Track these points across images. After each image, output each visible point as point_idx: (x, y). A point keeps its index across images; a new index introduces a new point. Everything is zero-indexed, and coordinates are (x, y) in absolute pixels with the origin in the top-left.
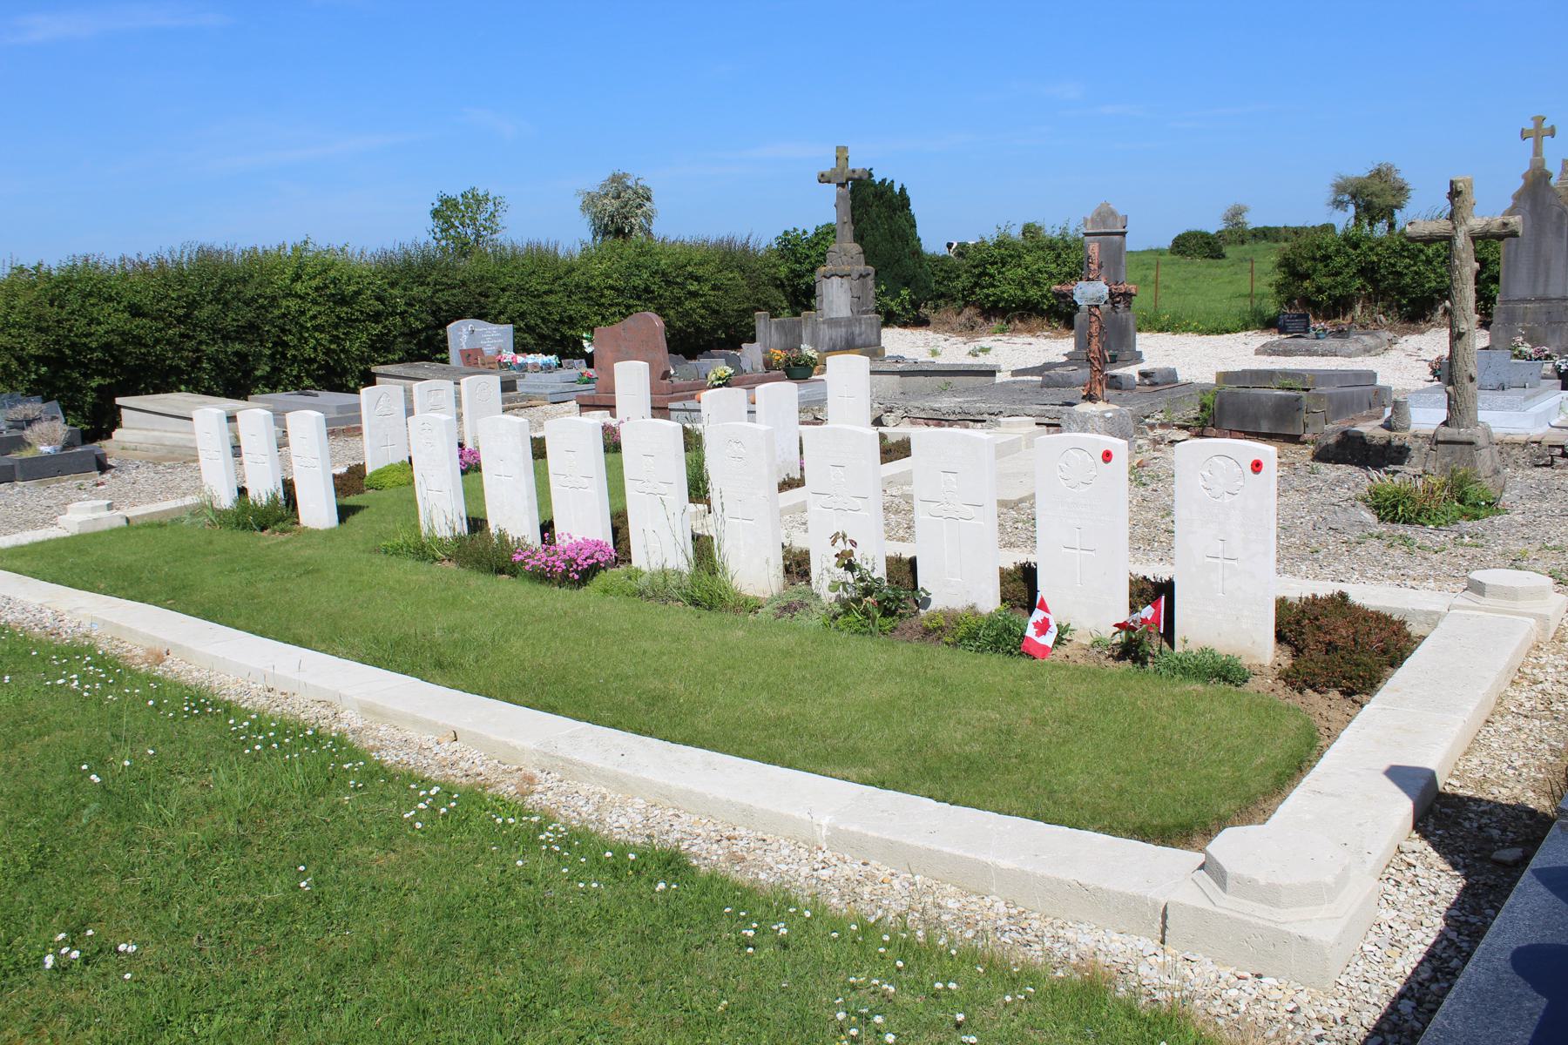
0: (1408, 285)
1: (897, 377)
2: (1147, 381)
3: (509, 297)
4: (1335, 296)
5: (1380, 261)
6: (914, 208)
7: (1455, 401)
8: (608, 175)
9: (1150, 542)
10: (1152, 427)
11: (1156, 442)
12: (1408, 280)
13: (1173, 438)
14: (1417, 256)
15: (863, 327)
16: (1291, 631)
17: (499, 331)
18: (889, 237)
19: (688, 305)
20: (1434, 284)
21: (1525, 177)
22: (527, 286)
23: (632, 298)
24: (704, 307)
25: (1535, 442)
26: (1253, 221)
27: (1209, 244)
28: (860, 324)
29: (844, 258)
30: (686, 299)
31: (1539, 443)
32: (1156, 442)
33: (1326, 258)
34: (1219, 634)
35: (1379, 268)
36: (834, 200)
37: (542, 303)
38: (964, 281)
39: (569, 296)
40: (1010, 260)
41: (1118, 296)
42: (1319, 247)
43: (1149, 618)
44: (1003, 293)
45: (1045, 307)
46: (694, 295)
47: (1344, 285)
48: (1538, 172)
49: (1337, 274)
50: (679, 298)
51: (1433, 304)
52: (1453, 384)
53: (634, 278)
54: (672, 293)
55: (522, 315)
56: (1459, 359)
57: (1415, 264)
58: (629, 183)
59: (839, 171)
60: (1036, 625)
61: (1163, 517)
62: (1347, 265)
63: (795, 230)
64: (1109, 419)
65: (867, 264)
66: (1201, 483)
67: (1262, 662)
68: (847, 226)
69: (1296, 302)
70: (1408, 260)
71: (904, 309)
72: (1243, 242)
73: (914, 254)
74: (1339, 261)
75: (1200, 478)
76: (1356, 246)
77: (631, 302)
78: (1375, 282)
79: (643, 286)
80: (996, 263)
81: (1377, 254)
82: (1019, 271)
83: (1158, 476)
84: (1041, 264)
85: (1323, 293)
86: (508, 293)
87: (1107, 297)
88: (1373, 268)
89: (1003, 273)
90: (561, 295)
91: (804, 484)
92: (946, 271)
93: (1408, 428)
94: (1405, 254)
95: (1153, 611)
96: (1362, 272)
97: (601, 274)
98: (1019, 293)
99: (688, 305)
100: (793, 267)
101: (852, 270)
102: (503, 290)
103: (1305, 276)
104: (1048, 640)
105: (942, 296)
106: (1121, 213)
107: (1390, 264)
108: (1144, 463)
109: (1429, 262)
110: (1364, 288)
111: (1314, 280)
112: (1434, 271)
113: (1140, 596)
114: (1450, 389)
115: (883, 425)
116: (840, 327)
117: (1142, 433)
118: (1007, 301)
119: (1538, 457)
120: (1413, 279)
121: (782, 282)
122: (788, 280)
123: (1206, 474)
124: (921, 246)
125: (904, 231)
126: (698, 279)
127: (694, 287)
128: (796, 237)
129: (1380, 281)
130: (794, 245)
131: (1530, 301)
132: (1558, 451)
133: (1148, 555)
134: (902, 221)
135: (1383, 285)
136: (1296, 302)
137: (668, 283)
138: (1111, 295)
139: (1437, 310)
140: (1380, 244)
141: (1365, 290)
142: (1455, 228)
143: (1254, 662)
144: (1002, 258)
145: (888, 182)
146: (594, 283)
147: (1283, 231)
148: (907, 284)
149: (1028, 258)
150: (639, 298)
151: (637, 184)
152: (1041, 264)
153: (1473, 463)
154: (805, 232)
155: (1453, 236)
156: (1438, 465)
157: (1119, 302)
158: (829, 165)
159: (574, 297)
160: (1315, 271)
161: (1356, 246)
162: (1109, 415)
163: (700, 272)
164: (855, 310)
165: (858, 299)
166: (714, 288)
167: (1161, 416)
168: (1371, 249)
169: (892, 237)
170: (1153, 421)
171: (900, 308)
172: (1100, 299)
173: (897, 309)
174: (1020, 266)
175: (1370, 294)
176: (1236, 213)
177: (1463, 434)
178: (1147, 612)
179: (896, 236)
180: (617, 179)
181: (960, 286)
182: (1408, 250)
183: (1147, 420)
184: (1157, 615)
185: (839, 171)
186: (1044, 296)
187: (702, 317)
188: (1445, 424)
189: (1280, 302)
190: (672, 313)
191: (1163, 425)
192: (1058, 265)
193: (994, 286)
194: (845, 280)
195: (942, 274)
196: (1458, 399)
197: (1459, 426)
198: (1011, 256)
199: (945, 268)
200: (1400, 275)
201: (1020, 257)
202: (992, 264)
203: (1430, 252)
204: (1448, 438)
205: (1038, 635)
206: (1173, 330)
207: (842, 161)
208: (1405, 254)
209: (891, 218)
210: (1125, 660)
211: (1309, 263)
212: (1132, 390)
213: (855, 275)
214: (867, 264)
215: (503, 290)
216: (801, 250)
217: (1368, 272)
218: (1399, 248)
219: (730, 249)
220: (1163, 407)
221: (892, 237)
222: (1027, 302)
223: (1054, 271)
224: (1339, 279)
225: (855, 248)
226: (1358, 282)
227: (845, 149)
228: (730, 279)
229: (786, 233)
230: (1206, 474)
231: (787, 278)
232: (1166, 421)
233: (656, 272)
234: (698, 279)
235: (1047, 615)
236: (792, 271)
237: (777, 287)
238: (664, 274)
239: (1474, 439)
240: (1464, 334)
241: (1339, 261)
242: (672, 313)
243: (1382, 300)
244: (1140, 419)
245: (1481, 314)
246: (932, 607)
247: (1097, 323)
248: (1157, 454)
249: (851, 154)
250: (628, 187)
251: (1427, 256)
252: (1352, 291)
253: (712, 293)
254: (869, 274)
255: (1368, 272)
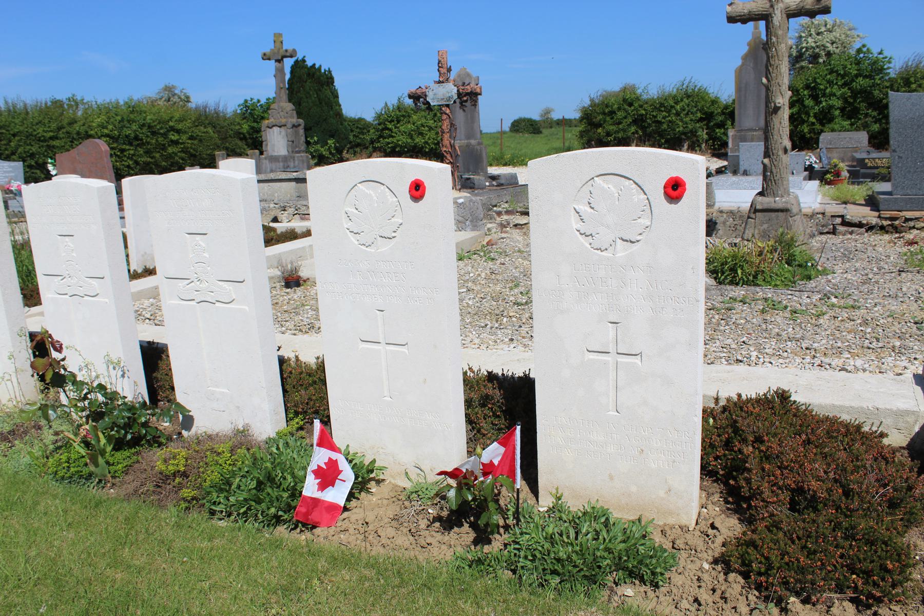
0: (665, 130)
1: (293, 184)
2: (494, 183)
3: (19, 141)
4: (618, 137)
5: (647, 114)
6: (337, 83)
7: (771, 172)
8: (162, 86)
9: (498, 317)
10: (499, 214)
11: (503, 226)
12: (665, 126)
13: (517, 222)
14: (670, 111)
15: (297, 162)
16: (717, 458)
17: (10, 167)
18: (318, 103)
19: (170, 150)
20: (681, 129)
21: (749, 44)
22: (35, 133)
23: (125, 144)
24: (182, 151)
25: (819, 214)
26: (556, 116)
27: (532, 125)
28: (294, 160)
29: (282, 114)
30: (169, 146)
31: (823, 214)
32: (503, 226)
33: (612, 113)
34: (611, 478)
35: (646, 119)
36: (273, 72)
37: (48, 146)
38: (372, 134)
39: (72, 142)
40: (402, 118)
41: (465, 96)
42: (607, 106)
43: (496, 462)
44: (398, 141)
45: (427, 150)
46: (176, 143)
47: (624, 130)
48: (757, 40)
49: (620, 123)
50: (164, 145)
51: (681, 143)
52: (769, 157)
53: (125, 129)
54: (157, 140)
55: (32, 156)
56: (775, 132)
57: (669, 116)
58: (176, 92)
59: (276, 51)
60: (318, 473)
61: (511, 289)
62: (625, 117)
63: (252, 99)
64: (460, 204)
65: (298, 118)
66: (576, 224)
67: (684, 522)
68: (283, 91)
69: (593, 143)
70: (664, 113)
71: (331, 153)
72: (551, 127)
73: (336, 115)
74: (620, 114)
75: (574, 218)
76: (630, 105)
77: (124, 147)
78: (643, 128)
79: (133, 135)
80: (393, 121)
81: (645, 110)
82: (409, 126)
83: (505, 252)
84: (424, 121)
85: (611, 136)
86: (17, 138)
87: (455, 97)
88: (642, 119)
89: (398, 128)
90: (63, 140)
91: (155, 274)
92: (360, 128)
93: (714, 205)
94: (663, 109)
95: (502, 450)
96: (635, 122)
97: (99, 126)
98: (409, 141)
99: (170, 150)
100: (252, 124)
101: (287, 122)
102: (14, 135)
103: (599, 125)
104: (337, 495)
105: (358, 145)
106: (474, 75)
107: (653, 115)
108: (492, 242)
109: (678, 114)
110: (637, 132)
111: (604, 127)
112: (681, 120)
113: (483, 405)
114: (766, 161)
115: (278, 222)
116: (279, 162)
117: (491, 219)
118: (401, 147)
119: (823, 226)
120: (668, 125)
121: (244, 135)
122: (249, 134)
123: (584, 208)
124: (341, 109)
125: (329, 99)
126: (178, 132)
127: (174, 137)
128: (253, 104)
129: (647, 127)
130: (252, 110)
131: (755, 130)
132: (839, 220)
133: (495, 334)
134: (328, 92)
135: (649, 130)
136: (593, 143)
137: (154, 133)
138: (459, 95)
139: (683, 146)
140: (647, 103)
141: (638, 134)
142: (772, 6)
143: (671, 521)
144: (397, 118)
145: (317, 66)
146: (92, 132)
147: (574, 121)
148: (332, 136)
149: (414, 117)
150: (131, 144)
151: (181, 92)
152: (424, 121)
153: (789, 227)
154: (259, 101)
155: (770, 14)
156: (757, 231)
157: (466, 101)
158: (268, 47)
159: (75, 142)
160: (605, 121)
161: (630, 105)
162: (461, 201)
163: (180, 127)
164: (290, 150)
165: (292, 143)
166: (191, 138)
167: (506, 205)
168: (641, 106)
169: (321, 103)
170: (500, 209)
171: (328, 153)
172: (450, 98)
173: (326, 153)
174: (409, 122)
175: (640, 137)
176: (548, 112)
177: (778, 202)
178: (493, 453)
179: (323, 104)
180: (169, 89)
181: (368, 138)
182: (664, 107)
183: (495, 208)
184: (509, 458)
185: (276, 51)
186: (426, 143)
187: (183, 159)
188: (761, 194)
189: (583, 143)
190: (157, 155)
191: (508, 212)
192: (435, 121)
193: (393, 137)
194: (282, 129)
195: (358, 130)
196: (774, 171)
197: (775, 195)
198: (403, 116)
199: (360, 126)
200: (660, 123)
201: (409, 116)
202: (390, 122)
203: (678, 107)
204: (766, 206)
205: (323, 487)
206: (513, 165)
207: (278, 44)
208: (663, 109)
209: (320, 90)
210: (460, 525)
211: (601, 117)
212: (482, 189)
213: (289, 125)
214: (298, 118)
215: (14, 135)
216: (257, 113)
217: (639, 121)
218: (658, 106)
219: (205, 111)
220: (508, 198)
221: (321, 103)
222: (415, 147)
223: (433, 125)
224: (621, 126)
225: (290, 106)
226: (633, 129)
227: (280, 35)
228: (204, 133)
229: (246, 101)
230: (584, 208)
231: (248, 132)
232: (510, 209)
233: (143, 125)
234: (178, 132)
235: (334, 456)
236: (252, 128)
237: (241, 139)
238: (150, 127)
239: (789, 206)
240: (779, 108)
241: (620, 114)
242: (157, 155)
243: (649, 140)
244: (489, 208)
245: (711, 149)
246: (194, 430)
247: (448, 121)
248: (503, 235)
249: (285, 39)
250: (175, 94)
251: (677, 111)
252: (630, 134)
253: (189, 141)
254: (299, 125)
255: (639, 121)
